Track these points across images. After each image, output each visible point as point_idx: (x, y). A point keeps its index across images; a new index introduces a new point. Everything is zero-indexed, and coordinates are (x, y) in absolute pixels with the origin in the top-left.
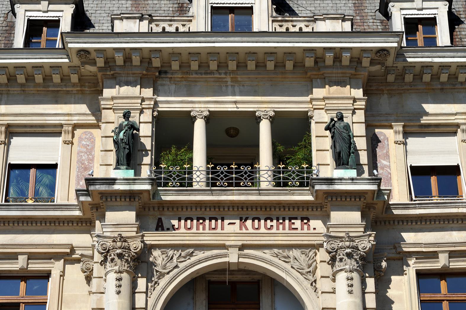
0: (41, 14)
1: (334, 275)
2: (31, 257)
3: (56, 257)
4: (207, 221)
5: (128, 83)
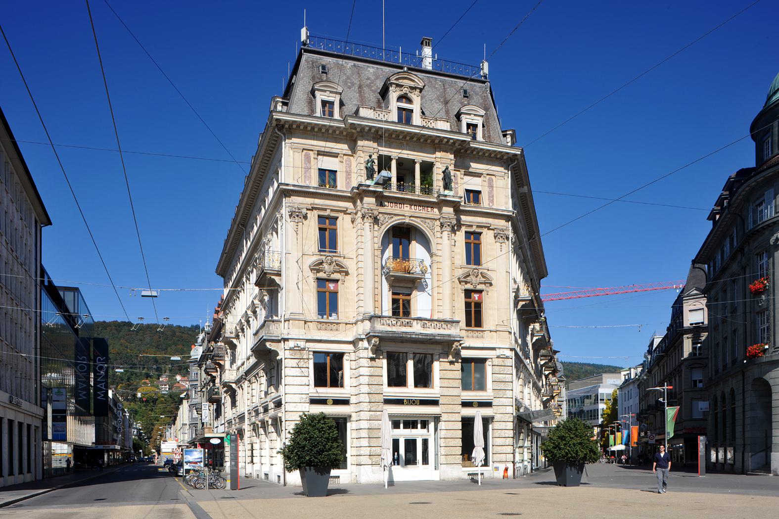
0: (471, 120)
1: (442, 232)
2: (332, 210)
3: (341, 211)
4: (398, 205)
5: (368, 140)
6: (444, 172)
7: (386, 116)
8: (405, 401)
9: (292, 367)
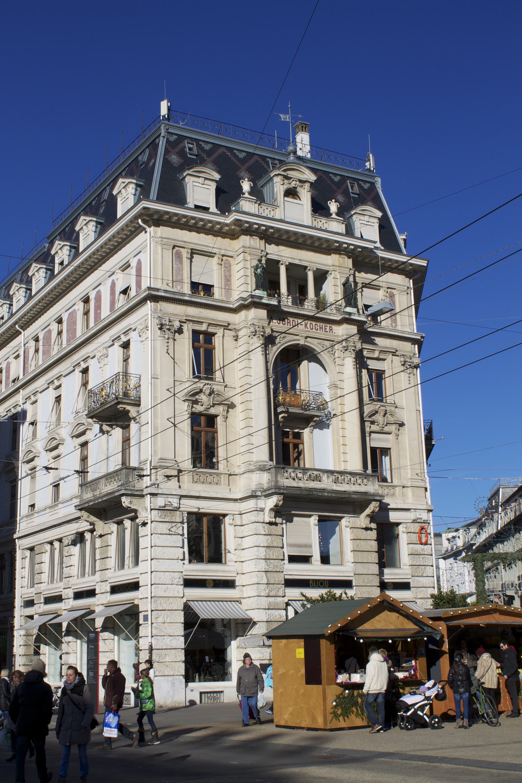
6: (344, 285)
7: (272, 212)
8: (310, 583)
9: (161, 534)
